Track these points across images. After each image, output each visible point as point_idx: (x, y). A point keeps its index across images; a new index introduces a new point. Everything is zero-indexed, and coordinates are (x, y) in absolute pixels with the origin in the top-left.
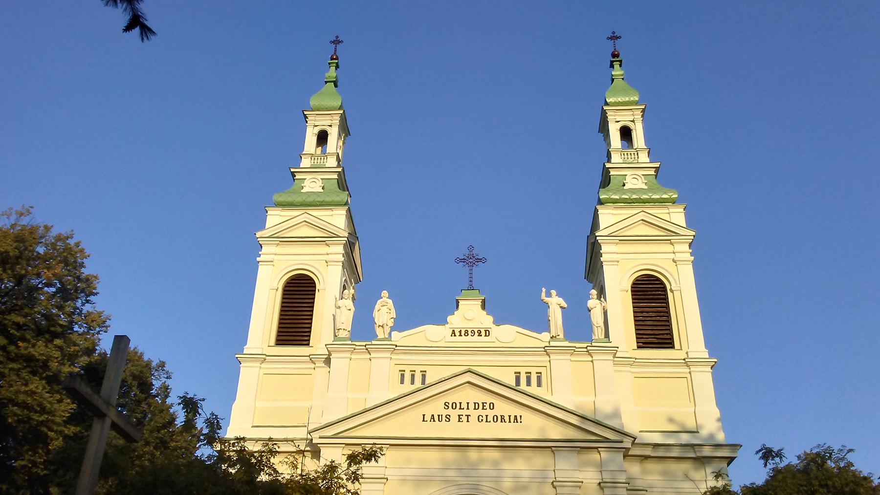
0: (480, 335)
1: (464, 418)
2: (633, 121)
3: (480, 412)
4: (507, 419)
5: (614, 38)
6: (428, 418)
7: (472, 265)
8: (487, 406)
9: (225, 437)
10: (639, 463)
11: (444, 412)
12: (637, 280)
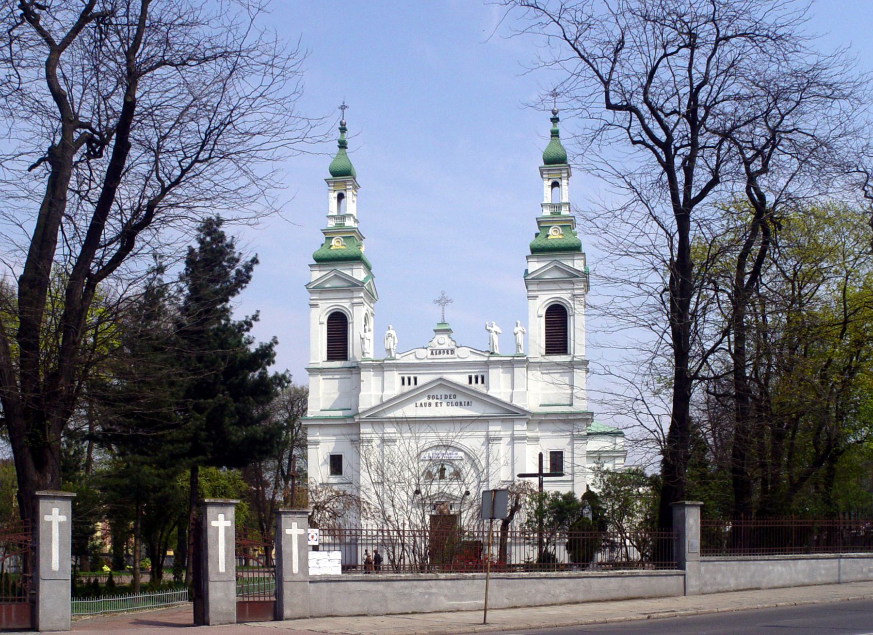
0: (448, 354)
1: (439, 405)
2: (560, 178)
3: (448, 400)
4: (463, 404)
5: (443, 301)
6: (418, 405)
7: (443, 305)
8: (452, 397)
9: (362, 407)
10: (537, 425)
11: (428, 401)
12: (550, 307)
